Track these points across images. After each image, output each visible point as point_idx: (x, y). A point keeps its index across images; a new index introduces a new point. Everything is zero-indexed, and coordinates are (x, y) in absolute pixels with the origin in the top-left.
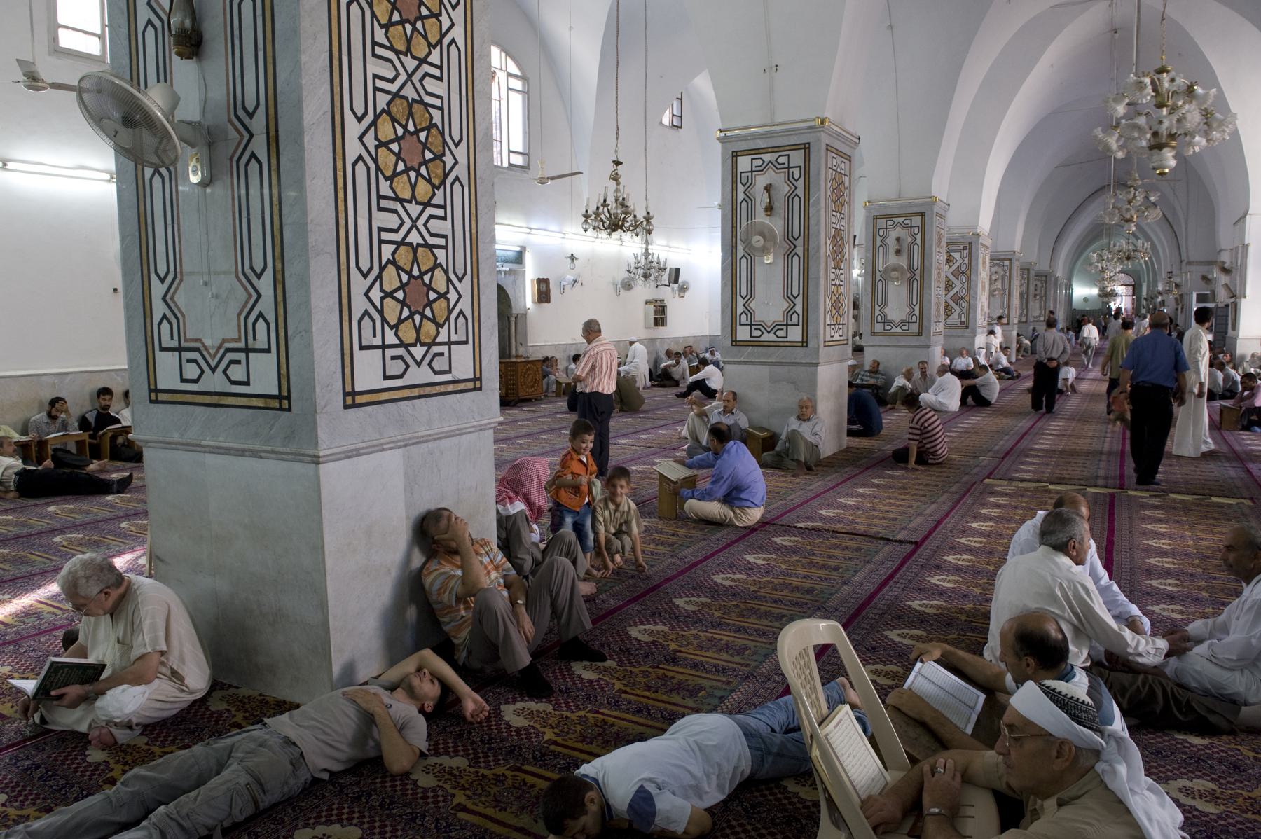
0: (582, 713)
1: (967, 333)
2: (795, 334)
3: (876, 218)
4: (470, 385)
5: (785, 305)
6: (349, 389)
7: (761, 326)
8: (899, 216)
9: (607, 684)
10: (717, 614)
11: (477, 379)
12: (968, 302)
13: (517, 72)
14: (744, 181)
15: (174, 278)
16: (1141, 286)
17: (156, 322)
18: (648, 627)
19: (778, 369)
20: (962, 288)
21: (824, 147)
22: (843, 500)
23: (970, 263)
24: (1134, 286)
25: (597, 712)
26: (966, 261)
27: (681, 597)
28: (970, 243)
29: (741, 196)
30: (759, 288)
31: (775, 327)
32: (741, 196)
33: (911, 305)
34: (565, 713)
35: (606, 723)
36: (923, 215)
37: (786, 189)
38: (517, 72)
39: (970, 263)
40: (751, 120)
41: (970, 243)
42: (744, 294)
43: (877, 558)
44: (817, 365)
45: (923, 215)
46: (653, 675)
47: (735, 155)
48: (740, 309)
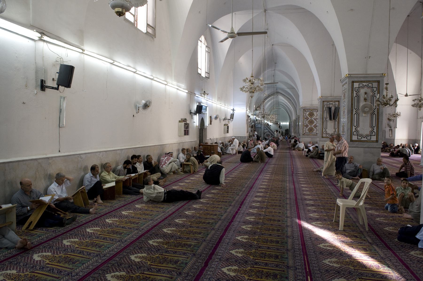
0: (138, 274)
2: (374, 138)
3: (323, 102)
5: (370, 129)
7: (362, 136)
8: (331, 101)
9: (145, 263)
10: (179, 234)
13: (199, 41)
14: (356, 90)
15: (358, 125)
18: (156, 240)
19: (367, 149)
25: (143, 273)
27: (165, 228)
29: (355, 95)
30: (361, 124)
31: (366, 136)
32: (355, 95)
33: (335, 128)
34: (131, 275)
35: (147, 277)
36: (339, 101)
38: (199, 41)
40: (359, 71)
42: (355, 125)
43: (228, 210)
45: (339, 101)
46: (161, 258)
47: (353, 82)
48: (354, 130)
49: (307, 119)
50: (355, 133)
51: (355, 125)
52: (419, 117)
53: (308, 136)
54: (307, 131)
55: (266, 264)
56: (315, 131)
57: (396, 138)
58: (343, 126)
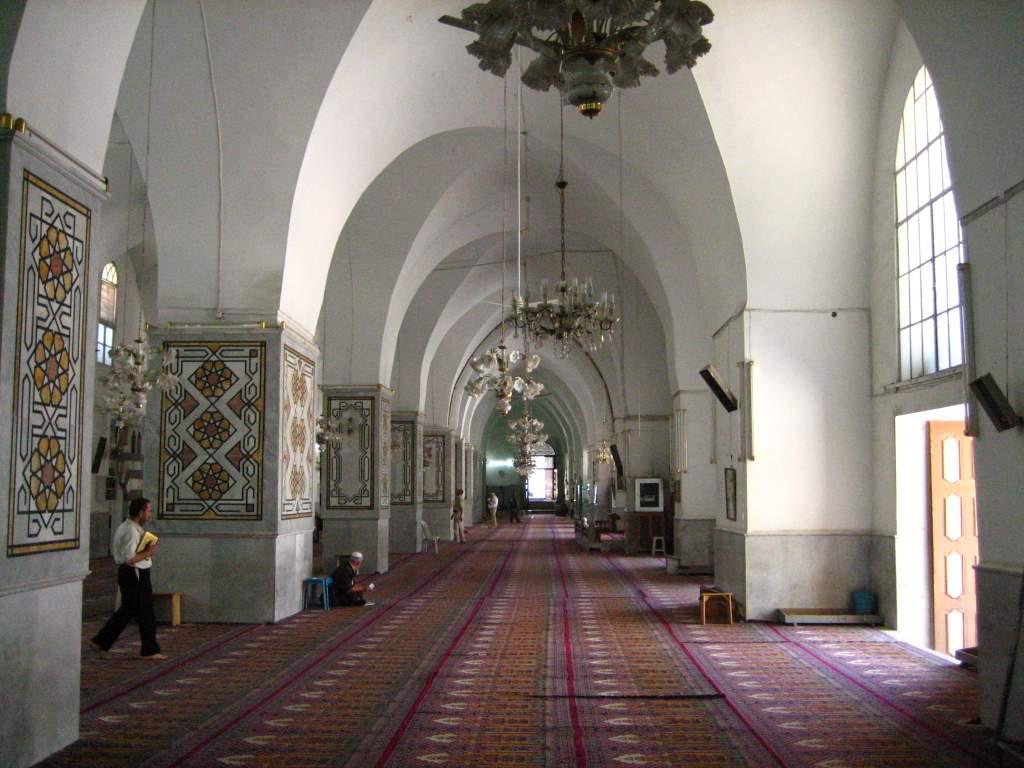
1: (259, 528)
4: (72, 544)
6: (10, 544)
11: (77, 539)
12: (261, 465)
15: (339, 480)
16: (562, 456)
17: (17, 491)
20: (248, 436)
21: (282, 346)
22: (290, 708)
23: (263, 386)
24: (554, 457)
26: (256, 379)
28: (263, 344)
30: (344, 475)
37: (361, 421)
39: (263, 386)
41: (263, 344)
44: (377, 519)
49: (187, 404)
50: (334, 493)
51: (334, 478)
52: (878, 389)
53: (194, 526)
54: (187, 493)
55: (285, 457)
56: (236, 493)
57: (751, 529)
58: (182, 511)
